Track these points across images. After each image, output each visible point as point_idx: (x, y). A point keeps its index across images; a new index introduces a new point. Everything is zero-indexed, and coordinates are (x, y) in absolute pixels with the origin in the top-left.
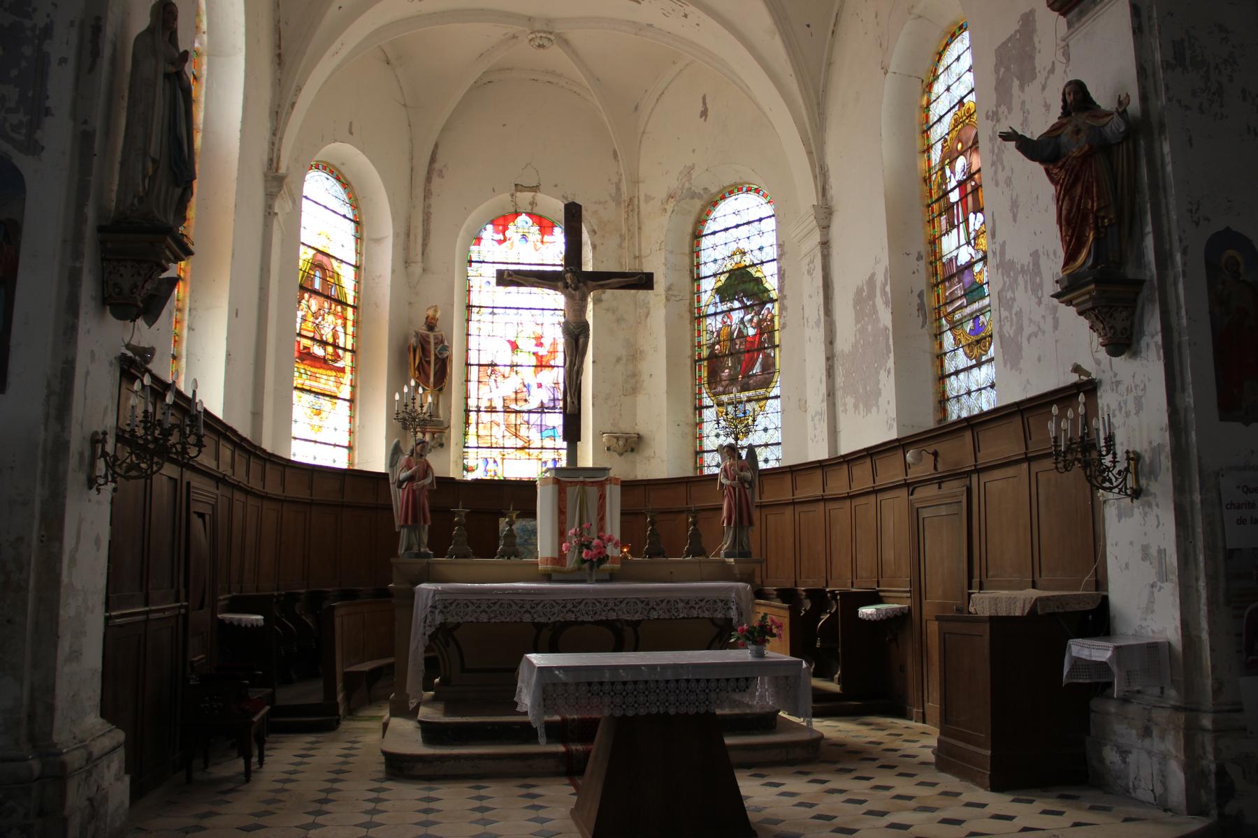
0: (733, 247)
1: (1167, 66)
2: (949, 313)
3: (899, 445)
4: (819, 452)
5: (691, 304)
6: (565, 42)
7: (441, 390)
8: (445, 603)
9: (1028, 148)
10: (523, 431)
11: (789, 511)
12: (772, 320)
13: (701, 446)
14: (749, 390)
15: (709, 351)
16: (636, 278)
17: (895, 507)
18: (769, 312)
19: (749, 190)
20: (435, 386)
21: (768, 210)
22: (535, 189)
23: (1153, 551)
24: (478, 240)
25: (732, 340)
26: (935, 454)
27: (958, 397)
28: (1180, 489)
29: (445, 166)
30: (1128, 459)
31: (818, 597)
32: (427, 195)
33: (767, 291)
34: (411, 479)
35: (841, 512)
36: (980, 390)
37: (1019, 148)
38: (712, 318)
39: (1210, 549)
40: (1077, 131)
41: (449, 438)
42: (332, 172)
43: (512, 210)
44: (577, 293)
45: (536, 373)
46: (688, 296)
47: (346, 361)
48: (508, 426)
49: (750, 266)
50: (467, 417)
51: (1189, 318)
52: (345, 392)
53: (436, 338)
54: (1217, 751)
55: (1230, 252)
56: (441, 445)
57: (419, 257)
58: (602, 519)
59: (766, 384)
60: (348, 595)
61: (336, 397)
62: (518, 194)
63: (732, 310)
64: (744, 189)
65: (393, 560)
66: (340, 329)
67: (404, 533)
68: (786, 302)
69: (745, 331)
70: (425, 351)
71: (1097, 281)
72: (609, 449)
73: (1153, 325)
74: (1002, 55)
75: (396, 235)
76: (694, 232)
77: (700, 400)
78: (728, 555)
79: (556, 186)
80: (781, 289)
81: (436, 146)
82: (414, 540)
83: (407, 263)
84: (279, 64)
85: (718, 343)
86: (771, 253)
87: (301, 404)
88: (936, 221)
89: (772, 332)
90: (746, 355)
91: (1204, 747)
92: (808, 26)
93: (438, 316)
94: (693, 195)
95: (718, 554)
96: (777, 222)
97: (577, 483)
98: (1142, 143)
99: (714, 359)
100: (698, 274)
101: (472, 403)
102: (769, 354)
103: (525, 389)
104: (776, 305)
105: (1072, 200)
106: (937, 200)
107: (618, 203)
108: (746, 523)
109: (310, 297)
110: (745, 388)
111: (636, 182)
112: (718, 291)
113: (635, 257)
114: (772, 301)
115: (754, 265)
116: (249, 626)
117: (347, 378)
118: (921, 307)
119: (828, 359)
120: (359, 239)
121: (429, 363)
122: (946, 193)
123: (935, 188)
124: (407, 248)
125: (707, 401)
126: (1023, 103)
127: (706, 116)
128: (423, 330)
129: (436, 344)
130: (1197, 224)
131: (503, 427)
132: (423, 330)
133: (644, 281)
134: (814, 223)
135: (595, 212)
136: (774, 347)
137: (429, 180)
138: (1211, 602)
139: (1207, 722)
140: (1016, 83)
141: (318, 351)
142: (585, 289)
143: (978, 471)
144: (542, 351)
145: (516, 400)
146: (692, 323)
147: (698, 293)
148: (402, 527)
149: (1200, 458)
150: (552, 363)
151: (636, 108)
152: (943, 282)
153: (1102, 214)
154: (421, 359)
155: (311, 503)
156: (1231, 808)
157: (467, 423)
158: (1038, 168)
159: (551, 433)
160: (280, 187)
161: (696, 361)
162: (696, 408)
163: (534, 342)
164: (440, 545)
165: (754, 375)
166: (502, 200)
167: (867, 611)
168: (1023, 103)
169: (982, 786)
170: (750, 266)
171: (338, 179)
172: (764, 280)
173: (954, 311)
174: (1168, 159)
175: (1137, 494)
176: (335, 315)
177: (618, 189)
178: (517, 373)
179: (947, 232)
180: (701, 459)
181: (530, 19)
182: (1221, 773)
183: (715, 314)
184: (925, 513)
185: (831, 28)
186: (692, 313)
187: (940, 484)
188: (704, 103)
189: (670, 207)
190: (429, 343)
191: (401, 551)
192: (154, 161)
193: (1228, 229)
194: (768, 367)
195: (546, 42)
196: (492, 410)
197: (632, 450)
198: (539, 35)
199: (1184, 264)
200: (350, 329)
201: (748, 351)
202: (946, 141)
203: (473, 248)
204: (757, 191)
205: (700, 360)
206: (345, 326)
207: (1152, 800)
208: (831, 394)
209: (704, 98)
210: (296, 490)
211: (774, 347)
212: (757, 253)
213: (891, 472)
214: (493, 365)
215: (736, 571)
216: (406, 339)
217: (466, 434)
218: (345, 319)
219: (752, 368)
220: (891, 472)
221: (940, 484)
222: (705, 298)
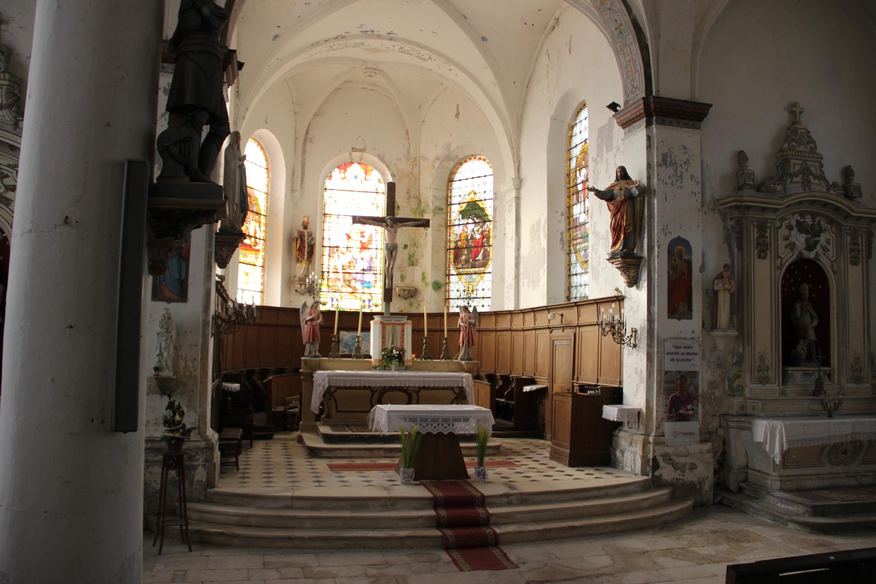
1: (659, 165)
2: (575, 245)
3: (547, 309)
4: (510, 306)
6: (381, 72)
7: (310, 261)
9: (600, 194)
10: (353, 284)
11: (493, 334)
12: (489, 232)
13: (449, 296)
14: (475, 267)
15: (455, 244)
16: (422, 221)
17: (544, 337)
18: (488, 227)
19: (480, 159)
20: (308, 260)
21: (490, 171)
22: (363, 150)
23: (639, 371)
25: (467, 240)
26: (562, 315)
27: (576, 286)
28: (650, 346)
29: (313, 136)
30: (632, 331)
31: (505, 378)
32: (304, 152)
33: (487, 215)
34: (312, 320)
35: (519, 336)
36: (585, 285)
37: (596, 195)
38: (457, 227)
39: (659, 371)
40: (621, 189)
43: (350, 161)
44: (392, 230)
45: (361, 252)
47: (260, 246)
48: (344, 281)
49: (479, 201)
50: (323, 275)
51: (658, 275)
52: (260, 262)
53: (308, 233)
54: (654, 451)
55: (679, 247)
57: (299, 188)
59: (484, 265)
61: (255, 265)
62: (354, 153)
63: (468, 223)
64: (477, 158)
66: (258, 229)
67: (308, 346)
68: (496, 224)
69: (474, 236)
70: (302, 241)
71: (622, 257)
73: (644, 276)
74: (600, 130)
75: (287, 176)
76: (449, 179)
77: (449, 271)
78: (462, 359)
79: (374, 149)
80: (494, 217)
84: (238, 97)
85: (460, 241)
86: (490, 195)
88: (571, 197)
89: (488, 238)
90: (475, 249)
91: (650, 450)
92: (514, 83)
93: (309, 221)
95: (457, 359)
96: (494, 177)
97: (391, 324)
98: (646, 198)
99: (457, 248)
100: (450, 202)
102: (487, 250)
103: (354, 261)
104: (492, 223)
105: (616, 220)
106: (573, 186)
108: (471, 344)
110: (473, 267)
112: (461, 212)
114: (489, 221)
115: (481, 200)
116: (226, 389)
117: (261, 254)
118: (562, 240)
119: (516, 258)
121: (304, 247)
122: (576, 185)
123: (572, 180)
124: (293, 182)
125: (453, 272)
126: (607, 159)
127: (459, 116)
128: (301, 229)
129: (308, 237)
130: (666, 235)
131: (342, 281)
132: (301, 229)
133: (426, 224)
134: (513, 186)
135: (395, 165)
136: (489, 246)
137: (305, 144)
138: (658, 392)
139: (651, 439)
140: (605, 149)
142: (396, 227)
143: (579, 326)
144: (364, 240)
145: (350, 266)
148: (307, 343)
149: (658, 334)
150: (369, 247)
151: (420, 107)
152: (573, 228)
153: (627, 227)
154: (300, 245)
156: (657, 473)
158: (604, 203)
161: (447, 250)
162: (446, 275)
163: (360, 235)
165: (479, 260)
166: (345, 156)
167: (527, 389)
168: (607, 159)
169: (565, 465)
170: (479, 201)
172: (486, 210)
173: (576, 244)
174: (656, 206)
175: (635, 346)
176: (255, 220)
177: (408, 152)
178: (350, 251)
179: (576, 204)
180: (449, 303)
181: (365, 61)
182: (655, 459)
183: (459, 225)
184: (556, 343)
185: (527, 84)
186: (446, 222)
187: (563, 329)
190: (304, 236)
192: (237, 205)
193: (679, 237)
194: (486, 256)
195: (372, 74)
197: (412, 297)
198: (369, 70)
199: (658, 252)
200: (263, 228)
201: (476, 247)
202: (578, 158)
204: (484, 160)
205: (450, 249)
206: (260, 226)
207: (630, 471)
208: (517, 276)
209: (458, 106)
211: (489, 246)
212: (482, 193)
213: (543, 319)
215: (466, 367)
218: (260, 222)
219: (477, 256)
220: (543, 319)
221: (563, 329)
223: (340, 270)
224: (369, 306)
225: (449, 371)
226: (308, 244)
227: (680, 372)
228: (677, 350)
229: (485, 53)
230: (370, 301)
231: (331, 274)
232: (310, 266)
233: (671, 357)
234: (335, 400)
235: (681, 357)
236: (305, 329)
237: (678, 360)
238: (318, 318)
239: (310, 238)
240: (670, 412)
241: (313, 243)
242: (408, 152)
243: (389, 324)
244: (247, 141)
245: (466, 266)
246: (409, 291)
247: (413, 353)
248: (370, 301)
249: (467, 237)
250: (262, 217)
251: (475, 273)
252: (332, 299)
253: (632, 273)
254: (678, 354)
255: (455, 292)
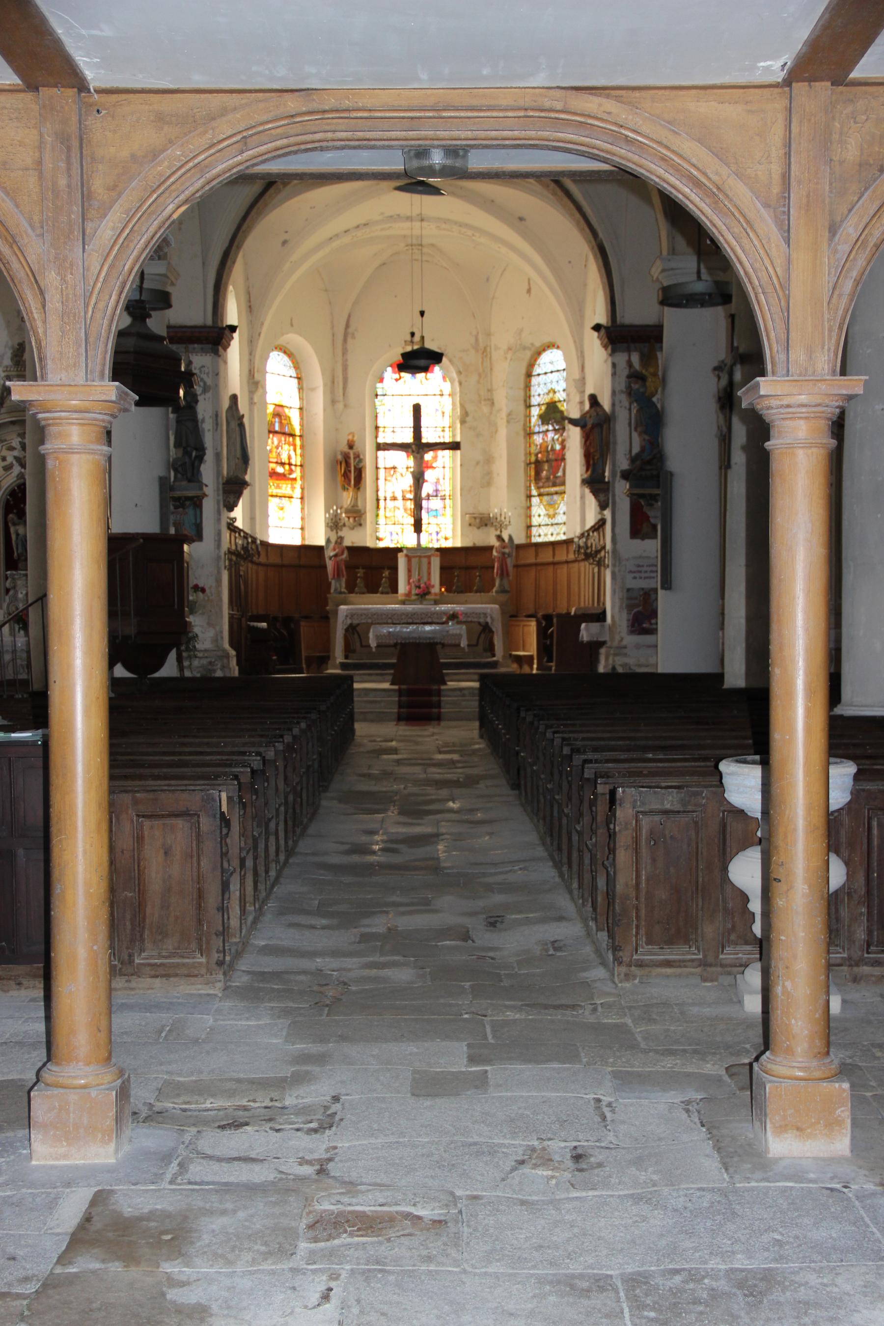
0: (549, 386)
5: (525, 425)
7: (359, 489)
8: (351, 615)
24: (381, 380)
25: (548, 452)
32: (345, 352)
34: (336, 556)
41: (365, 520)
42: (281, 349)
44: (418, 456)
46: (522, 419)
47: (297, 474)
52: (297, 493)
53: (354, 454)
56: (360, 525)
57: (341, 398)
58: (429, 574)
60: (306, 617)
61: (291, 497)
65: (328, 595)
67: (333, 582)
70: (348, 464)
72: (470, 525)
75: (325, 385)
77: (530, 491)
81: (349, 316)
82: (338, 586)
83: (333, 402)
85: (540, 452)
87: (273, 503)
93: (355, 439)
94: (525, 348)
99: (538, 464)
101: (381, 495)
107: (477, 351)
109: (280, 441)
110: (554, 485)
111: (489, 335)
113: (489, 390)
117: (299, 483)
120: (301, 389)
121: (350, 471)
125: (534, 492)
128: (346, 449)
129: (355, 458)
131: (402, 510)
132: (346, 449)
137: (345, 341)
141: (280, 470)
146: (525, 437)
147: (529, 416)
155: (283, 566)
157: (378, 507)
159: (434, 513)
160: (257, 387)
164: (351, 588)
171: (285, 352)
176: (289, 444)
177: (477, 340)
183: (539, 433)
186: (525, 430)
188: (529, 284)
189: (509, 355)
190: (349, 458)
191: (332, 591)
196: (394, 499)
200: (299, 451)
203: (379, 385)
205: (530, 463)
206: (295, 450)
210: (274, 559)
214: (394, 468)
216: (335, 456)
217: (377, 515)
218: (294, 445)
222: (534, 420)
223: (400, 497)
224: (438, 540)
225: (482, 603)
226: (355, 467)
227: (643, 589)
228: (640, 569)
229: (525, 234)
230: (437, 533)
231: (388, 501)
232: (359, 494)
233: (633, 575)
234: (359, 635)
235: (643, 575)
236: (330, 565)
237: (641, 578)
238: (342, 553)
239: (357, 460)
240: (633, 626)
241: (360, 466)
242: (477, 340)
243: (414, 557)
244: (266, 358)
245: (546, 484)
246: (481, 519)
247: (441, 585)
248: (437, 533)
249: (547, 447)
250: (298, 439)
251: (556, 493)
252: (391, 534)
253: (602, 497)
254: (640, 572)
255: (537, 517)
